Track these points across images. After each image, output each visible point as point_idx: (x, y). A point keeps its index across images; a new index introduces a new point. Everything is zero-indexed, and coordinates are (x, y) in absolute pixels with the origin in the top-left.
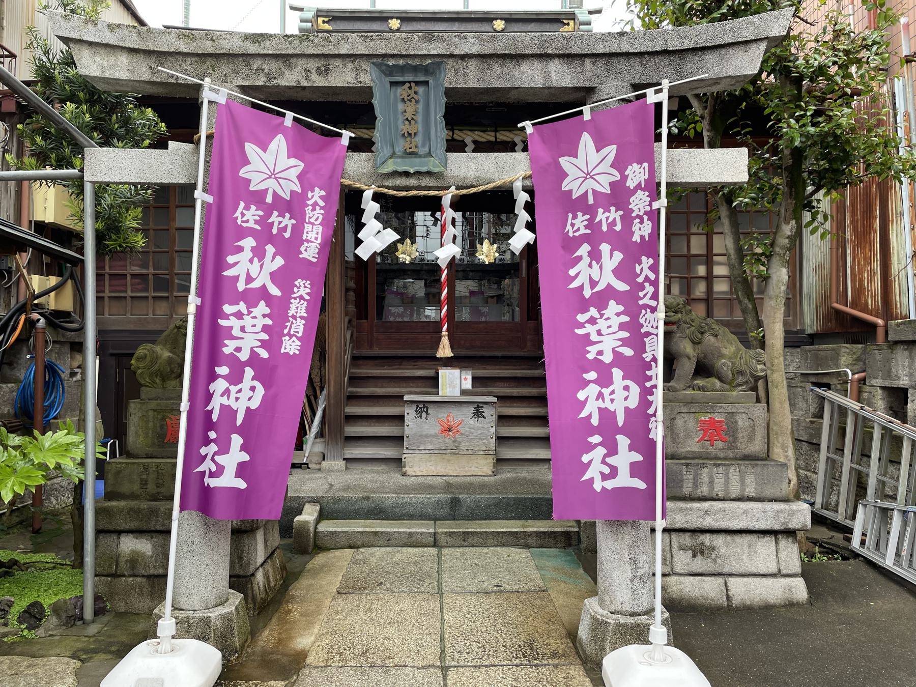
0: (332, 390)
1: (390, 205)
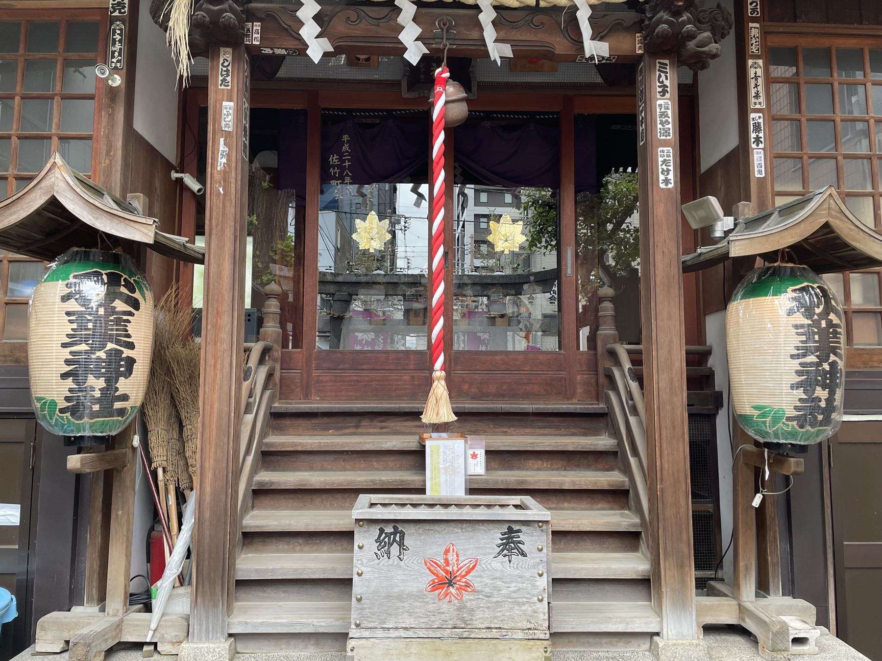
0: (208, 490)
1: (347, 164)
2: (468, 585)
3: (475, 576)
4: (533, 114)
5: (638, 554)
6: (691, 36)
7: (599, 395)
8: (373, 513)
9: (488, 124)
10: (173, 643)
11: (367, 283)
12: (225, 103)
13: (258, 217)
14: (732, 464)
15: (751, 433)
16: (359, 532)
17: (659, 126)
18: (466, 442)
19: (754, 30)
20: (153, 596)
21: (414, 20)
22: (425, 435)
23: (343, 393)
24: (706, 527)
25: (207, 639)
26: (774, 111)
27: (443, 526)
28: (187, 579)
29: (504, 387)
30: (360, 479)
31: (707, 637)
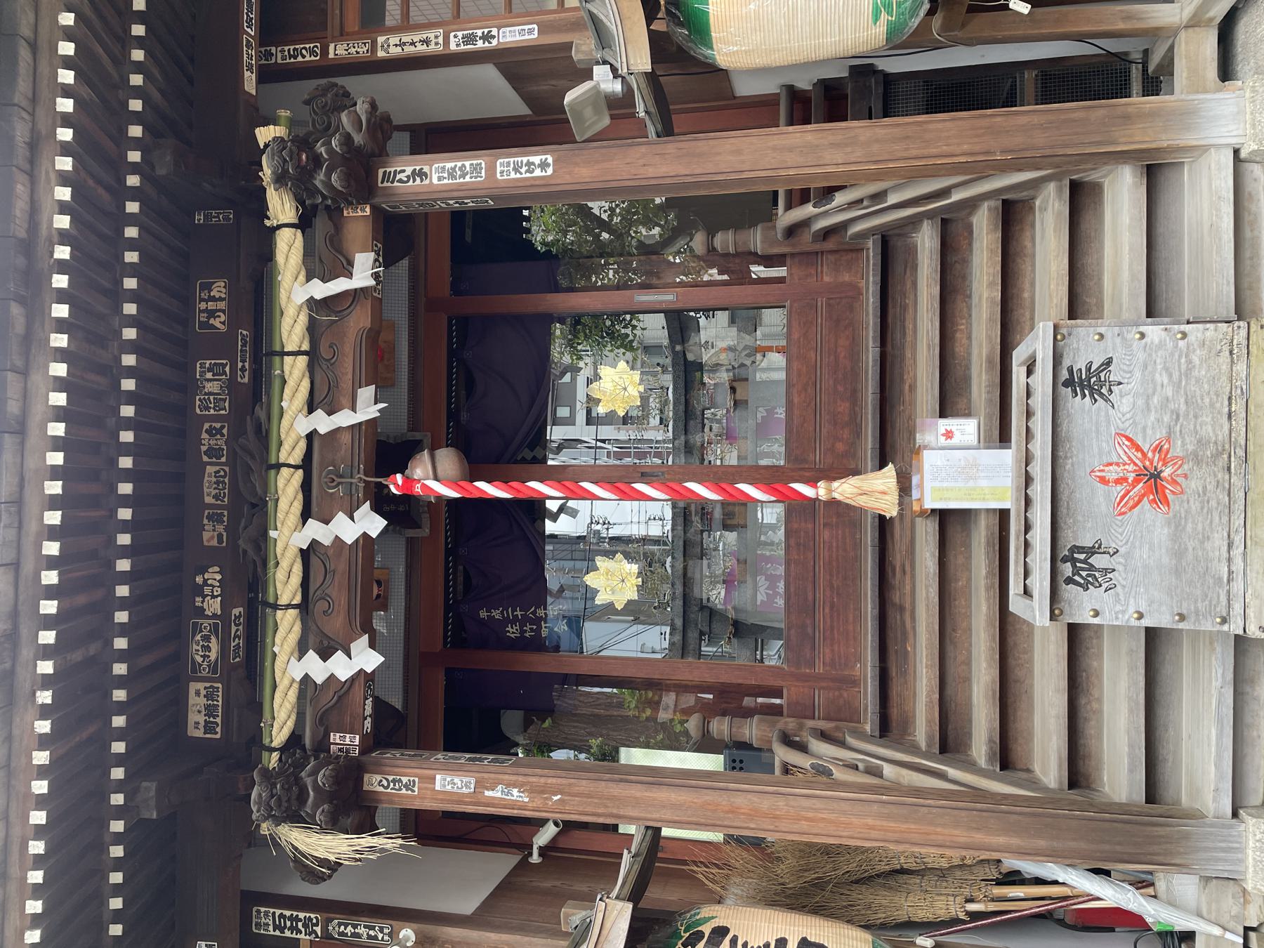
0: (1001, 840)
1: (519, 613)
2: (1158, 449)
3: (1144, 440)
4: (452, 354)
5: (1106, 184)
6: (348, 139)
7: (854, 249)
8: (1041, 594)
9: (464, 416)
10: (1246, 902)
11: (685, 585)
12: (438, 787)
13: (592, 735)
14: (961, 47)
15: (915, 22)
16: (1071, 615)
17: (468, 179)
18: (926, 447)
19: (338, 50)
20: (1169, 929)
21: (327, 522)
22: (916, 508)
23: (851, 628)
24: (1064, 82)
25: (1241, 850)
26: (447, 14)
27: (1062, 487)
28: (1144, 876)
29: (840, 389)
30: (984, 608)
31: (1240, 75)
